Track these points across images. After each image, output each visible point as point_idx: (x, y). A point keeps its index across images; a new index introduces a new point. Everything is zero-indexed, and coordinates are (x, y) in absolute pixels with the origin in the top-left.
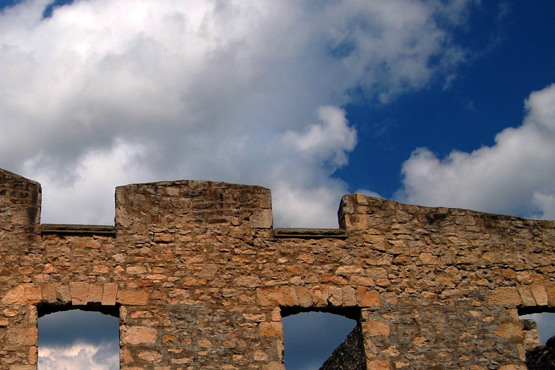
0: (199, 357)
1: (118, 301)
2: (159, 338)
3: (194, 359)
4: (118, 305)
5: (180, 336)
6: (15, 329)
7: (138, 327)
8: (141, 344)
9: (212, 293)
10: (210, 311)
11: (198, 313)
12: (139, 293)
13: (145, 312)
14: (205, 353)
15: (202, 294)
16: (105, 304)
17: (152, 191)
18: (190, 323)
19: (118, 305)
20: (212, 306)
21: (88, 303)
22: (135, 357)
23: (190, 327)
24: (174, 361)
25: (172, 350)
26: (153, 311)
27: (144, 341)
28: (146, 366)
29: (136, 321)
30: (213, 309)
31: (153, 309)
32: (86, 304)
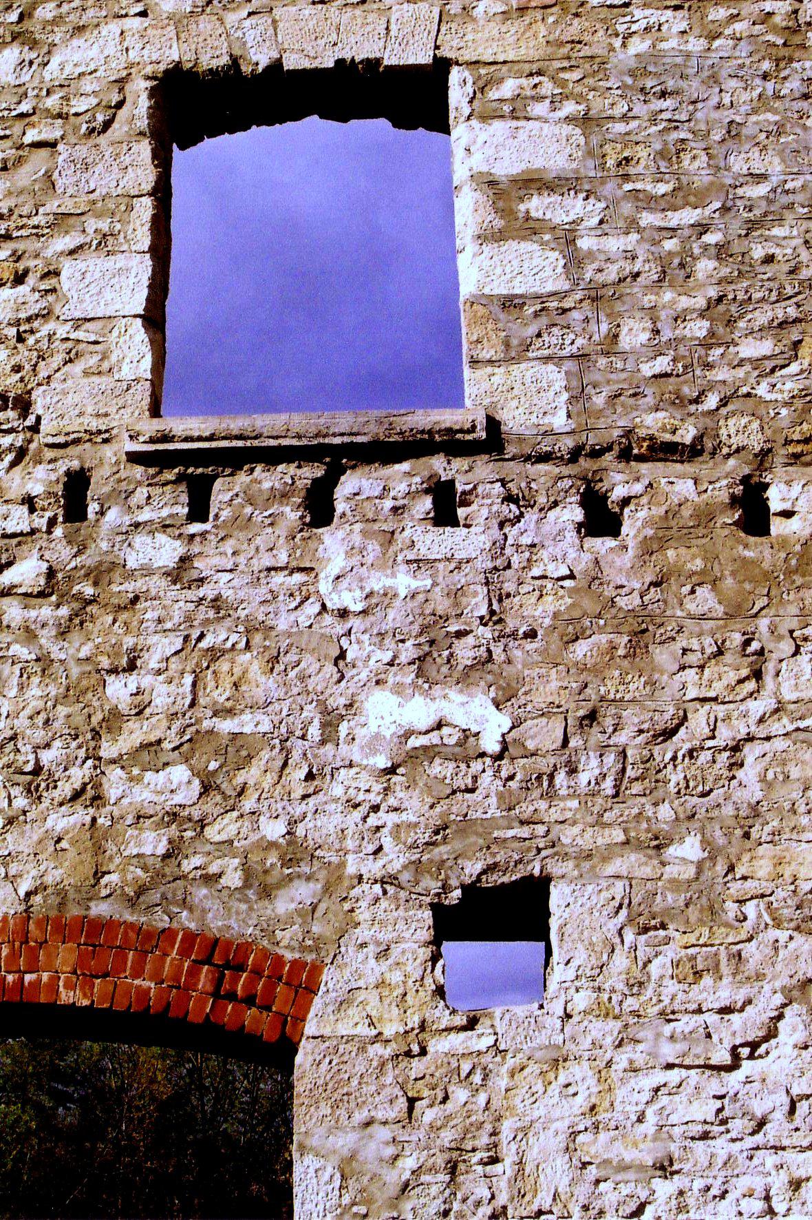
0: (739, 202)
1: (446, 52)
2: (595, 154)
3: (725, 209)
4: (442, 66)
5: (665, 143)
6: (85, 149)
7: (515, 123)
8: (528, 171)
9: (770, 14)
10: (766, 65)
11: (724, 73)
12: (516, 26)
13: (537, 80)
14: (762, 190)
15: (734, 18)
16: (306, 64)
17: (28, 423)
18: (700, 105)
19: (442, 66)
20: (774, 51)
21: (340, 62)
22: (506, 213)
23: (699, 115)
24: (648, 219)
25: (639, 186)
26: (566, 75)
27: (538, 163)
28: (547, 237)
29: (507, 108)
30: (778, 61)
31: (563, 69)
32: (331, 65)
